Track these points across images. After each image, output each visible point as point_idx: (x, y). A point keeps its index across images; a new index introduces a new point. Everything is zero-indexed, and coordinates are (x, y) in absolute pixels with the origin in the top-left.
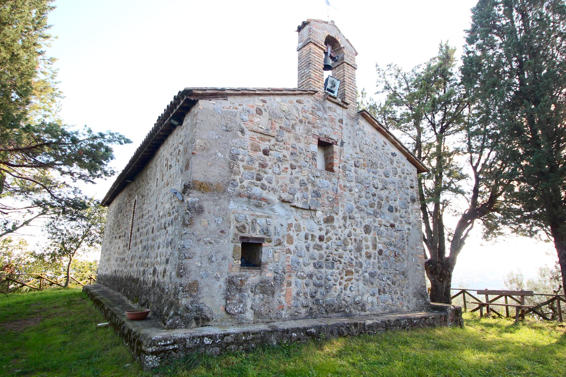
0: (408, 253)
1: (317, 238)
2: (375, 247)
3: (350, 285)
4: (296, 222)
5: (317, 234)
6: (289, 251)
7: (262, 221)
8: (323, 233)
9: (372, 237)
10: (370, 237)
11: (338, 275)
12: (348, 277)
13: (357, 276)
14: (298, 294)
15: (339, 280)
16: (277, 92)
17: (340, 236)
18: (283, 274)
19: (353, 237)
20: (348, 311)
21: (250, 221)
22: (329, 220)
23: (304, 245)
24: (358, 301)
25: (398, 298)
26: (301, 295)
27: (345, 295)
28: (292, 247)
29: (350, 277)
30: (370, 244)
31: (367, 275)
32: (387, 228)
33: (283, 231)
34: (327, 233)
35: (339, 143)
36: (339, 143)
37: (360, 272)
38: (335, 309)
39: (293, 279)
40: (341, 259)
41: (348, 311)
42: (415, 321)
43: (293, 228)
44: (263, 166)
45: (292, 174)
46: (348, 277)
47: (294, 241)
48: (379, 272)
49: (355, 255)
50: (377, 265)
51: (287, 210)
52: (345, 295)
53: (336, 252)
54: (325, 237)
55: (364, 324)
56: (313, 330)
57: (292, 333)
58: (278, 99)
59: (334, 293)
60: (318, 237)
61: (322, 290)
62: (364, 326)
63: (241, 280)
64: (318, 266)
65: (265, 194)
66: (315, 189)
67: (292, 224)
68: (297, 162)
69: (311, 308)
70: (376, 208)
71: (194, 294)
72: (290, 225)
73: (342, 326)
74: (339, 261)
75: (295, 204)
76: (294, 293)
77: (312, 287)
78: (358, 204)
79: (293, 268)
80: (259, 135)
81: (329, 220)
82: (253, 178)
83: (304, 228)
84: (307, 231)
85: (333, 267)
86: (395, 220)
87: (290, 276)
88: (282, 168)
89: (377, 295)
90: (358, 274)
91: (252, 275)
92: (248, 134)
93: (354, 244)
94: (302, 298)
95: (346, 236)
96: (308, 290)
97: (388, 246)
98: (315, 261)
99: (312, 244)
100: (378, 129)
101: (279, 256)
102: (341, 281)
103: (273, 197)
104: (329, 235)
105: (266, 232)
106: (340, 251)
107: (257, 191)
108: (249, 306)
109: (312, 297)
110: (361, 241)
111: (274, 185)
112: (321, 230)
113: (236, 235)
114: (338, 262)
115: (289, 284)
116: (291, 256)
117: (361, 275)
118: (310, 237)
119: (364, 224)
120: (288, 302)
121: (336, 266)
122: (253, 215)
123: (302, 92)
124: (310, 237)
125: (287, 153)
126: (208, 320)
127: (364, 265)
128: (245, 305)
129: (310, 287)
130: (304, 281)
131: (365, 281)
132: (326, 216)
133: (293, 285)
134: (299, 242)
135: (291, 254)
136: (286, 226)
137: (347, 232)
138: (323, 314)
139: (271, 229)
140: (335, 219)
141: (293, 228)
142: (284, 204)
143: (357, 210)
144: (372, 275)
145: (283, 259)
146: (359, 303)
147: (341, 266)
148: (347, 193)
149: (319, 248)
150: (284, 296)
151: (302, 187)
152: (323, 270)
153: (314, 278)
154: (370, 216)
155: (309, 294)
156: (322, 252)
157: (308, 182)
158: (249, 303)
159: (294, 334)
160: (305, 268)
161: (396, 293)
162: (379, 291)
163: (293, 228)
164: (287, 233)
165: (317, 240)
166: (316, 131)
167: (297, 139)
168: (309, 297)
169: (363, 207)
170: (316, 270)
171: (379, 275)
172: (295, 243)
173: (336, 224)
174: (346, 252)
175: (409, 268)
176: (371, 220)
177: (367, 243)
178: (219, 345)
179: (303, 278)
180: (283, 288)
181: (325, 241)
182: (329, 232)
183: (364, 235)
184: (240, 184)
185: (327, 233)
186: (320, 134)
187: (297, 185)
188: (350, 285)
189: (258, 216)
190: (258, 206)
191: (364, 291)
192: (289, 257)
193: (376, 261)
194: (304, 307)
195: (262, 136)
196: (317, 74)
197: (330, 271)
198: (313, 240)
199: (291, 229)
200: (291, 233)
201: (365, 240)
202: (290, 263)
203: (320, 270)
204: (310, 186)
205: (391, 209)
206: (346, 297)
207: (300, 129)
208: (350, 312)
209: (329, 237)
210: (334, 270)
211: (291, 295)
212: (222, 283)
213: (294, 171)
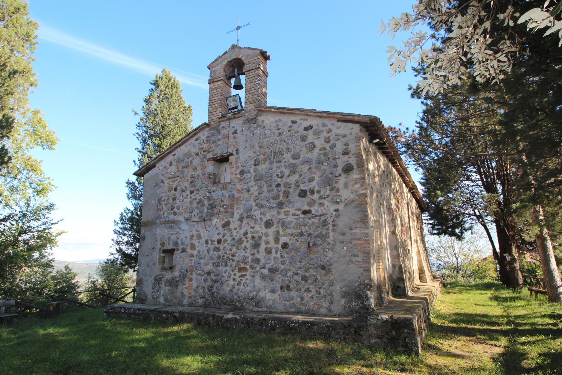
0: (334, 241)
1: (216, 242)
2: (277, 240)
3: (244, 281)
4: (197, 233)
5: (216, 238)
6: (192, 256)
7: (173, 237)
8: (221, 237)
9: (274, 231)
10: (271, 231)
11: (231, 272)
12: (241, 274)
13: (252, 272)
14: (197, 287)
15: (232, 276)
16: (178, 144)
17: (235, 237)
18: (186, 273)
19: (249, 235)
20: (239, 305)
21: (167, 238)
22: (226, 225)
23: (206, 249)
24: (251, 296)
25: (312, 298)
26: (199, 288)
27: (238, 290)
28: (195, 253)
29: (244, 273)
30: (271, 238)
31: (265, 271)
32: (297, 217)
33: (187, 241)
34: (223, 236)
35: (234, 153)
36: (234, 153)
37: (258, 269)
38: (226, 302)
39: (194, 276)
40: (234, 258)
41: (239, 305)
42: (292, 325)
43: (195, 238)
44: (174, 199)
45: (191, 198)
46: (241, 274)
47: (196, 247)
48: (282, 267)
49: (252, 252)
50: (280, 260)
51: (190, 225)
52: (238, 290)
53: (230, 252)
54: (223, 240)
55: (222, 317)
56: (177, 314)
57: (163, 314)
58: (182, 147)
59: (226, 288)
60: (216, 241)
61: (218, 285)
62: (222, 319)
63: (160, 277)
64: (216, 265)
65: (176, 218)
66: (211, 202)
67: (193, 235)
68: (195, 186)
69: (207, 299)
70: (281, 198)
71: (141, 285)
72: (192, 236)
73: (200, 315)
74: (232, 259)
75: (193, 219)
76: (194, 286)
77: (209, 283)
78: (257, 201)
79: (192, 269)
80: (171, 180)
81: (226, 225)
82: (169, 210)
83: (204, 236)
84: (206, 238)
85: (226, 265)
86: (309, 204)
87: (191, 274)
88: (184, 196)
89: (279, 292)
90: (253, 271)
91: (167, 274)
92: (166, 181)
93: (251, 241)
94: (200, 291)
95: (242, 236)
96: (206, 285)
97: (297, 238)
98: (214, 261)
99: (212, 247)
100: (162, 158)
101: (183, 260)
102: (235, 277)
103: (181, 218)
104: (226, 237)
105: (176, 243)
106: (234, 250)
107: (172, 217)
108: (162, 294)
109: (209, 290)
110: (260, 238)
111: (181, 210)
112: (219, 234)
113: (160, 249)
114: (231, 261)
115: (191, 280)
116: (194, 259)
117: (257, 272)
118: (210, 242)
119: (265, 220)
120: (190, 293)
121: (229, 264)
122: (168, 234)
123: (195, 132)
124: (210, 242)
125: (187, 184)
126: (145, 301)
127: (263, 261)
128: (160, 293)
129: (208, 283)
130: (203, 278)
131: (264, 277)
132: (224, 222)
133: (194, 281)
134: (200, 247)
135: (194, 257)
136: (189, 237)
137: (242, 231)
138: (216, 305)
139: (179, 242)
140: (231, 222)
141: (195, 238)
142: (188, 222)
143: (257, 208)
144: (273, 271)
145: (186, 261)
146: (253, 299)
147: (234, 264)
148: (246, 195)
149: (217, 249)
150: (187, 288)
151: (199, 205)
152: (220, 268)
153: (212, 275)
154: (273, 209)
155: (206, 288)
156: (220, 253)
157: (205, 199)
158: (162, 291)
159: (164, 315)
160: (205, 267)
161: (308, 290)
162: (282, 288)
163: (195, 238)
164: (190, 242)
165: (216, 244)
166: (210, 156)
167: (195, 169)
168: (206, 290)
169: (264, 202)
170: (215, 268)
171: (282, 271)
172: (197, 249)
173: (232, 226)
174: (240, 251)
175: (336, 259)
176: (275, 212)
177: (267, 239)
178: (127, 314)
179: (202, 275)
180: (185, 283)
181: (222, 243)
182: (226, 235)
183: (264, 230)
184: (163, 216)
185: (223, 236)
186: (214, 155)
187: (195, 205)
188: (244, 281)
189: (172, 234)
190: (171, 227)
191: (261, 287)
192: (192, 260)
193: (279, 255)
194: (201, 298)
195: (174, 179)
196: (214, 106)
197: (224, 269)
198: (212, 244)
199: (194, 238)
200: (194, 242)
201: (265, 236)
202: (193, 264)
203: (217, 268)
204: (206, 202)
205: (303, 194)
206: (239, 292)
207: (197, 161)
208: (242, 306)
209: (226, 239)
210: (228, 268)
211: (192, 288)
212: (152, 279)
213: (192, 195)
